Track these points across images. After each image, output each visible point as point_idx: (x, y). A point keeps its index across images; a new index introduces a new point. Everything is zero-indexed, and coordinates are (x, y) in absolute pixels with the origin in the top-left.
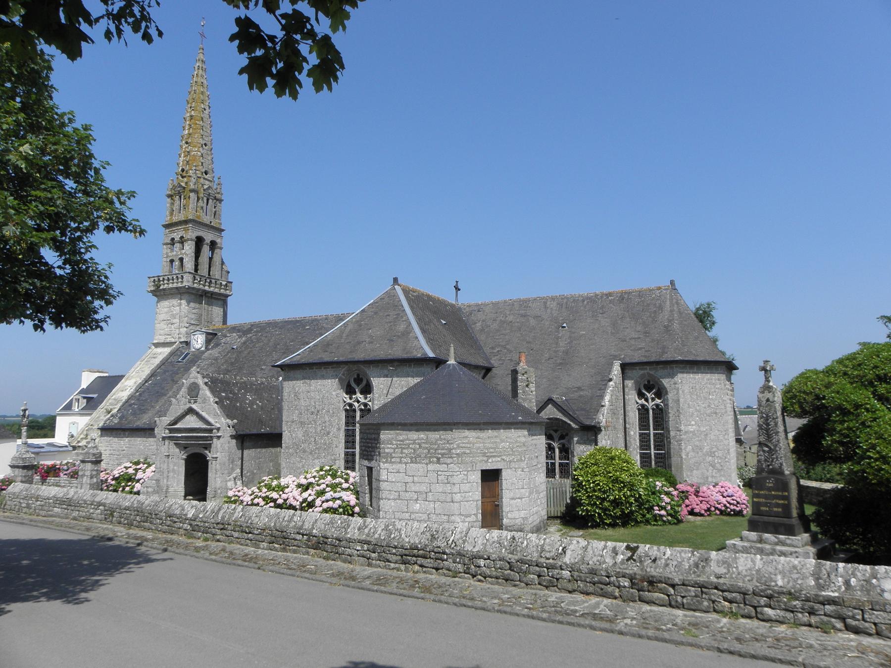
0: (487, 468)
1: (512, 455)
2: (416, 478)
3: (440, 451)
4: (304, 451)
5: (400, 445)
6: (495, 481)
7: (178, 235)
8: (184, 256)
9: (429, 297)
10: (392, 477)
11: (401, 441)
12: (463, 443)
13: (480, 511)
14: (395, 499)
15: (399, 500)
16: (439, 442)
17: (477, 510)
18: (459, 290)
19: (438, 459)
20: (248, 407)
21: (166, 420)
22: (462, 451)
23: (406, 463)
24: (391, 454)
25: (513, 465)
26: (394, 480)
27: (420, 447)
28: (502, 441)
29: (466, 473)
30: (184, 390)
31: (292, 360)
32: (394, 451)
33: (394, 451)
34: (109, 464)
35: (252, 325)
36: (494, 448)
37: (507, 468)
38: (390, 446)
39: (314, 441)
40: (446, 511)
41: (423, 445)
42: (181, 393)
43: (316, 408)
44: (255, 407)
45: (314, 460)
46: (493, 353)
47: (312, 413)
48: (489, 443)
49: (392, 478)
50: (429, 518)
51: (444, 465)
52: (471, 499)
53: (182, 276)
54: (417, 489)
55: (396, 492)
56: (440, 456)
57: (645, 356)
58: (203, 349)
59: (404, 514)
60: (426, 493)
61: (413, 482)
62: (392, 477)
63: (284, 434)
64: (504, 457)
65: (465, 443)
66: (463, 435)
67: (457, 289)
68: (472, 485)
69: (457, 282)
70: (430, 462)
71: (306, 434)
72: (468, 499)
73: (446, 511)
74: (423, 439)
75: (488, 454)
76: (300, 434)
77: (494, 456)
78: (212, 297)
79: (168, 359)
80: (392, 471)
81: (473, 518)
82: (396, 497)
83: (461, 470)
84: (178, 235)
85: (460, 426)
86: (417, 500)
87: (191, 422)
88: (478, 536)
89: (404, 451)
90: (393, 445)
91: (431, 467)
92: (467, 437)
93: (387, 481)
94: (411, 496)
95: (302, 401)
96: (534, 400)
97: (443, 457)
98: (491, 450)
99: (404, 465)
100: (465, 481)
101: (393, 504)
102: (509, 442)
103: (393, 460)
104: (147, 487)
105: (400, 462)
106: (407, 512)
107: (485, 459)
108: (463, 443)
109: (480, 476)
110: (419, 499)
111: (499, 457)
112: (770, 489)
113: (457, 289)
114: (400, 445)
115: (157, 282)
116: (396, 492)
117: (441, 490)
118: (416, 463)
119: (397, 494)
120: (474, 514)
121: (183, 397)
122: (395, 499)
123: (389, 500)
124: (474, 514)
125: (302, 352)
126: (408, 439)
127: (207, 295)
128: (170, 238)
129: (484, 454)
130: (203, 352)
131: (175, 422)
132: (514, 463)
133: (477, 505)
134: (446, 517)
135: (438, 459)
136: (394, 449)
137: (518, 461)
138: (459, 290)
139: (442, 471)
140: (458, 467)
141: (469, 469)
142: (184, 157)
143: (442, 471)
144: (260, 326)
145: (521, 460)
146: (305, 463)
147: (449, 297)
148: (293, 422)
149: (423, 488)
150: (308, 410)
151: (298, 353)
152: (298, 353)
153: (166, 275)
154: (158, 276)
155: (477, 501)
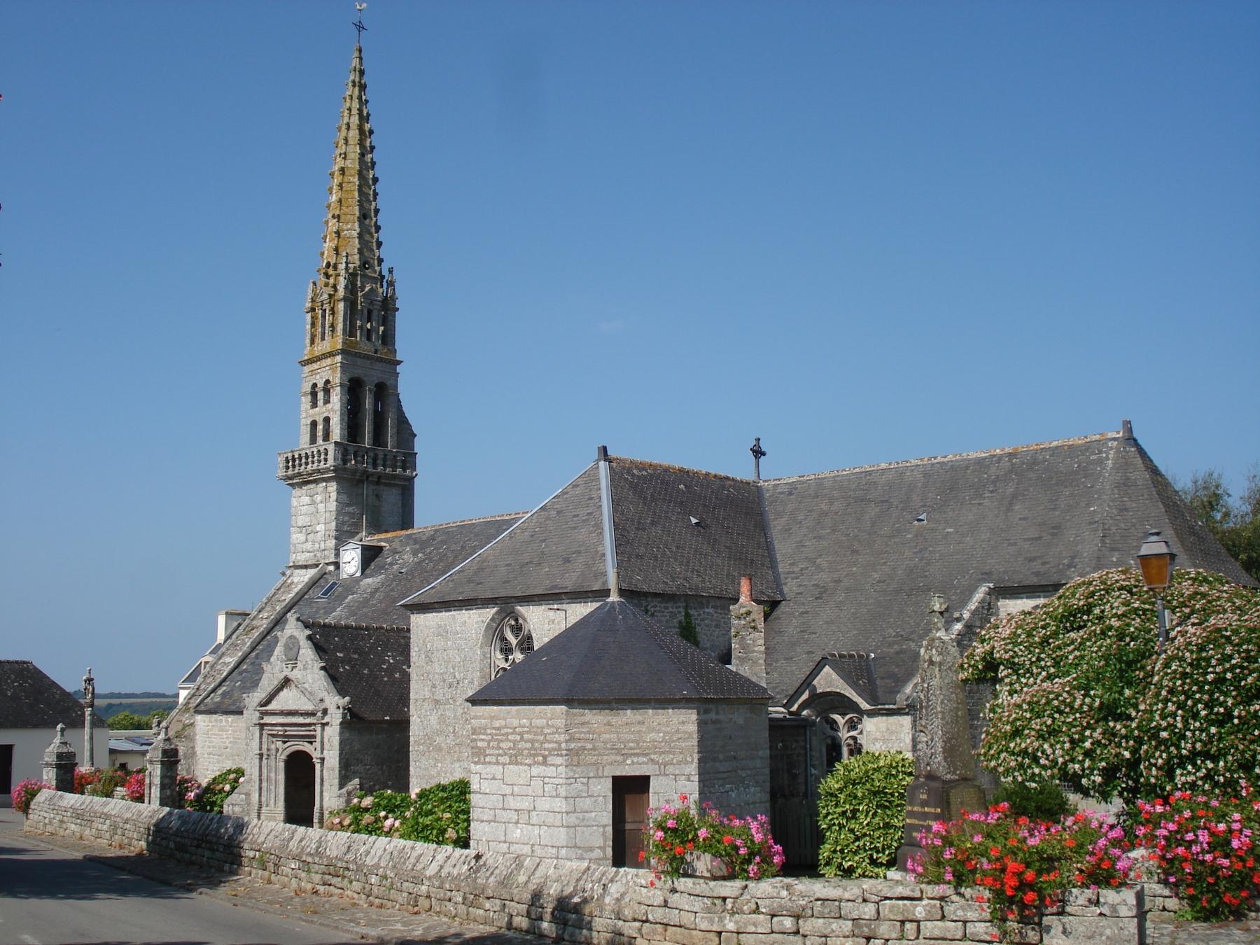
0: (624, 774)
1: (670, 752)
2: (516, 788)
3: (547, 745)
4: (440, 749)
5: (496, 735)
6: (644, 793)
7: (321, 378)
8: (331, 416)
9: (684, 474)
10: (486, 786)
11: (498, 729)
12: (582, 733)
13: (611, 843)
14: (489, 822)
15: (495, 822)
16: (546, 731)
17: (605, 841)
18: (763, 454)
19: (545, 757)
20: (384, 676)
21: (259, 695)
22: (579, 745)
23: (504, 764)
24: (485, 751)
25: (670, 769)
26: (488, 791)
27: (522, 738)
28: (653, 730)
29: (585, 780)
30: (279, 650)
31: (414, 600)
32: (489, 745)
33: (489, 745)
34: (208, 770)
35: (436, 531)
36: (637, 742)
37: (660, 775)
38: (482, 737)
39: (454, 732)
40: (554, 840)
41: (526, 736)
42: (276, 653)
43: (455, 677)
44: (397, 675)
45: (452, 764)
46: (793, 573)
47: (451, 686)
48: (626, 733)
49: (486, 788)
50: (533, 851)
51: (552, 767)
52: (594, 823)
53: (325, 449)
54: (518, 806)
55: (490, 809)
56: (547, 753)
57: (1037, 574)
58: (358, 574)
59: (501, 844)
60: (529, 811)
61: (512, 794)
62: (486, 786)
63: (412, 719)
64: (652, 756)
65: (584, 733)
66: (582, 719)
67: (758, 453)
68: (595, 801)
69: (758, 440)
70: (535, 763)
71: (442, 720)
72: (589, 823)
73: (554, 840)
74: (524, 726)
75: (626, 751)
76: (434, 720)
77: (637, 755)
78: (378, 483)
79: (305, 594)
80: (487, 777)
81: (597, 853)
82: (490, 818)
83: (577, 776)
84: (321, 378)
85: (576, 704)
86: (517, 823)
87: (288, 699)
88: (847, 926)
89: (502, 745)
90: (487, 735)
91: (536, 770)
92: (588, 723)
93: (480, 793)
94: (510, 816)
95: (436, 665)
96: (762, 661)
97: (550, 755)
98: (632, 745)
99: (501, 767)
100: (584, 795)
101: (486, 829)
102: (665, 733)
103: (488, 759)
104: (233, 804)
105: (497, 763)
106: (505, 842)
107: (620, 758)
108: (582, 733)
109: (611, 786)
110: (521, 821)
111: (645, 755)
112: (924, 804)
113: (758, 453)
114: (496, 735)
115: (291, 462)
116: (490, 809)
117: (547, 807)
118: (517, 763)
119: (492, 812)
120: (599, 848)
121: (278, 659)
122: (489, 822)
123: (482, 821)
124: (599, 848)
125: (440, 583)
126: (506, 727)
127: (370, 479)
128: (311, 383)
129: (618, 752)
130: (358, 581)
131: (268, 701)
132: (672, 767)
133: (604, 833)
134: (554, 851)
135: (545, 757)
136: (489, 742)
137: (679, 763)
138: (763, 454)
139: (549, 777)
140: (572, 770)
141: (592, 775)
142: (330, 241)
143: (549, 777)
144: (448, 532)
145: (687, 763)
146: (441, 768)
147: (740, 468)
148: (424, 701)
149: (525, 804)
150: (444, 681)
151: (433, 585)
152: (433, 585)
153: (303, 449)
154: (292, 452)
155: (604, 826)
